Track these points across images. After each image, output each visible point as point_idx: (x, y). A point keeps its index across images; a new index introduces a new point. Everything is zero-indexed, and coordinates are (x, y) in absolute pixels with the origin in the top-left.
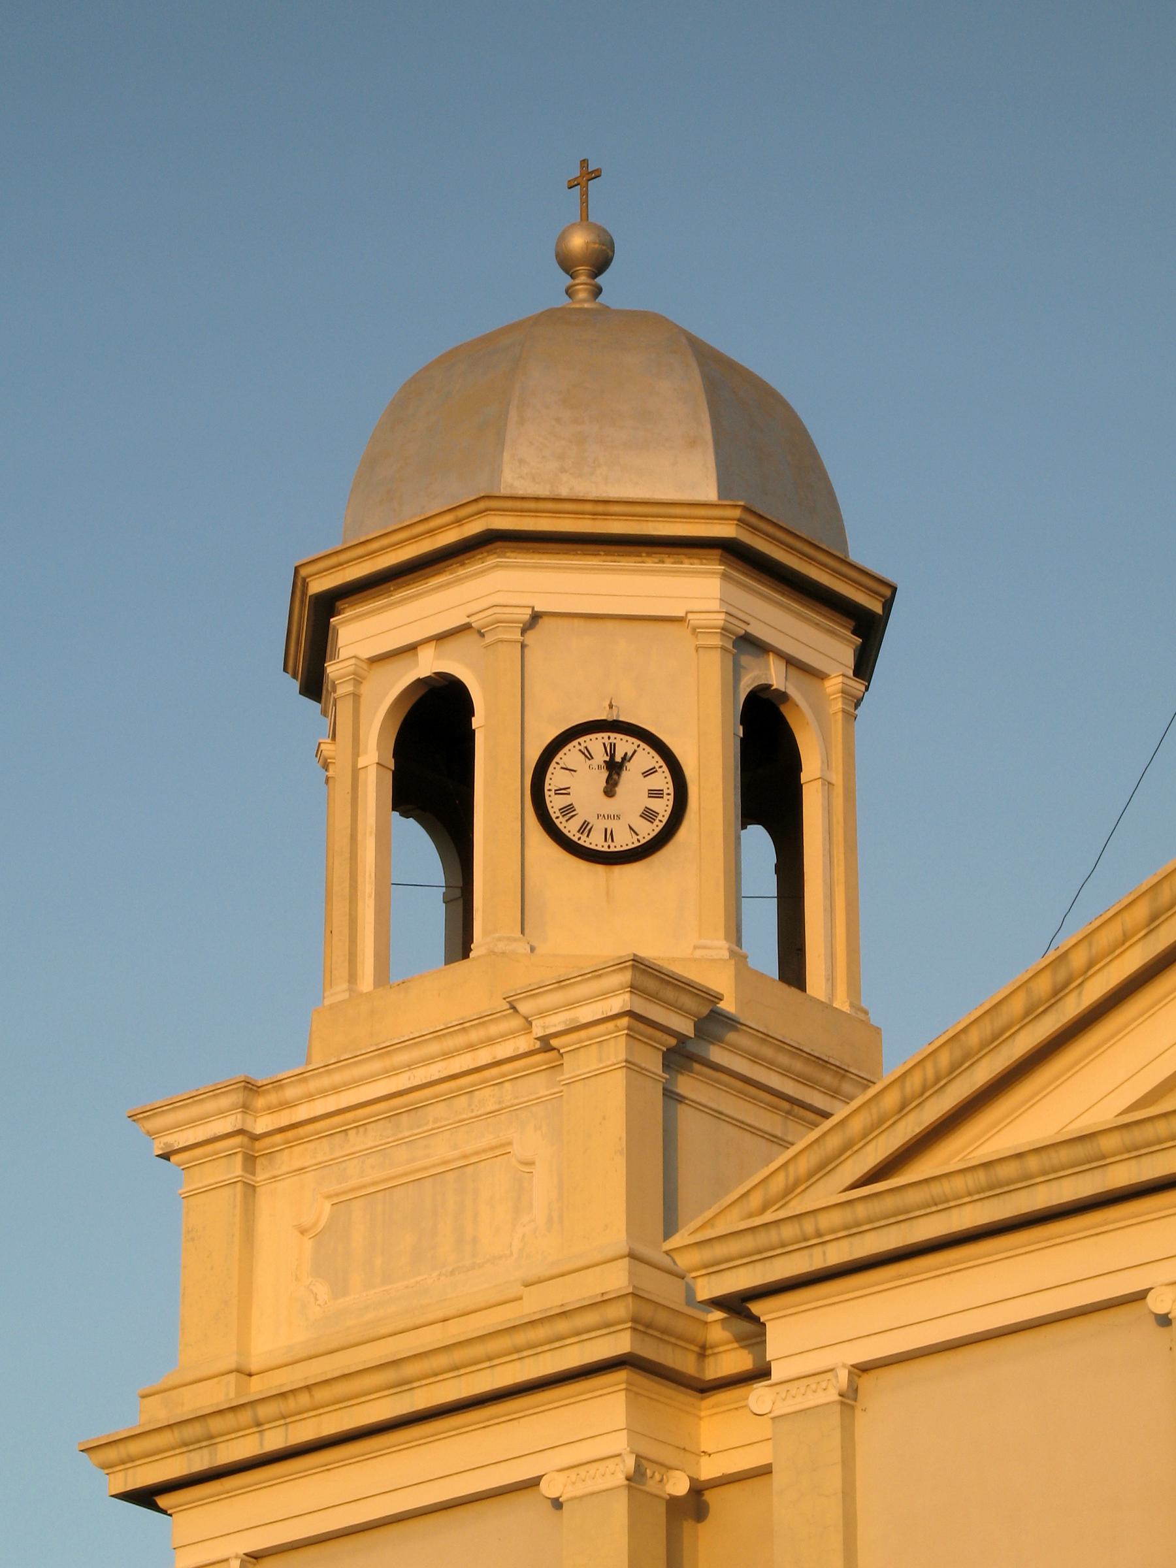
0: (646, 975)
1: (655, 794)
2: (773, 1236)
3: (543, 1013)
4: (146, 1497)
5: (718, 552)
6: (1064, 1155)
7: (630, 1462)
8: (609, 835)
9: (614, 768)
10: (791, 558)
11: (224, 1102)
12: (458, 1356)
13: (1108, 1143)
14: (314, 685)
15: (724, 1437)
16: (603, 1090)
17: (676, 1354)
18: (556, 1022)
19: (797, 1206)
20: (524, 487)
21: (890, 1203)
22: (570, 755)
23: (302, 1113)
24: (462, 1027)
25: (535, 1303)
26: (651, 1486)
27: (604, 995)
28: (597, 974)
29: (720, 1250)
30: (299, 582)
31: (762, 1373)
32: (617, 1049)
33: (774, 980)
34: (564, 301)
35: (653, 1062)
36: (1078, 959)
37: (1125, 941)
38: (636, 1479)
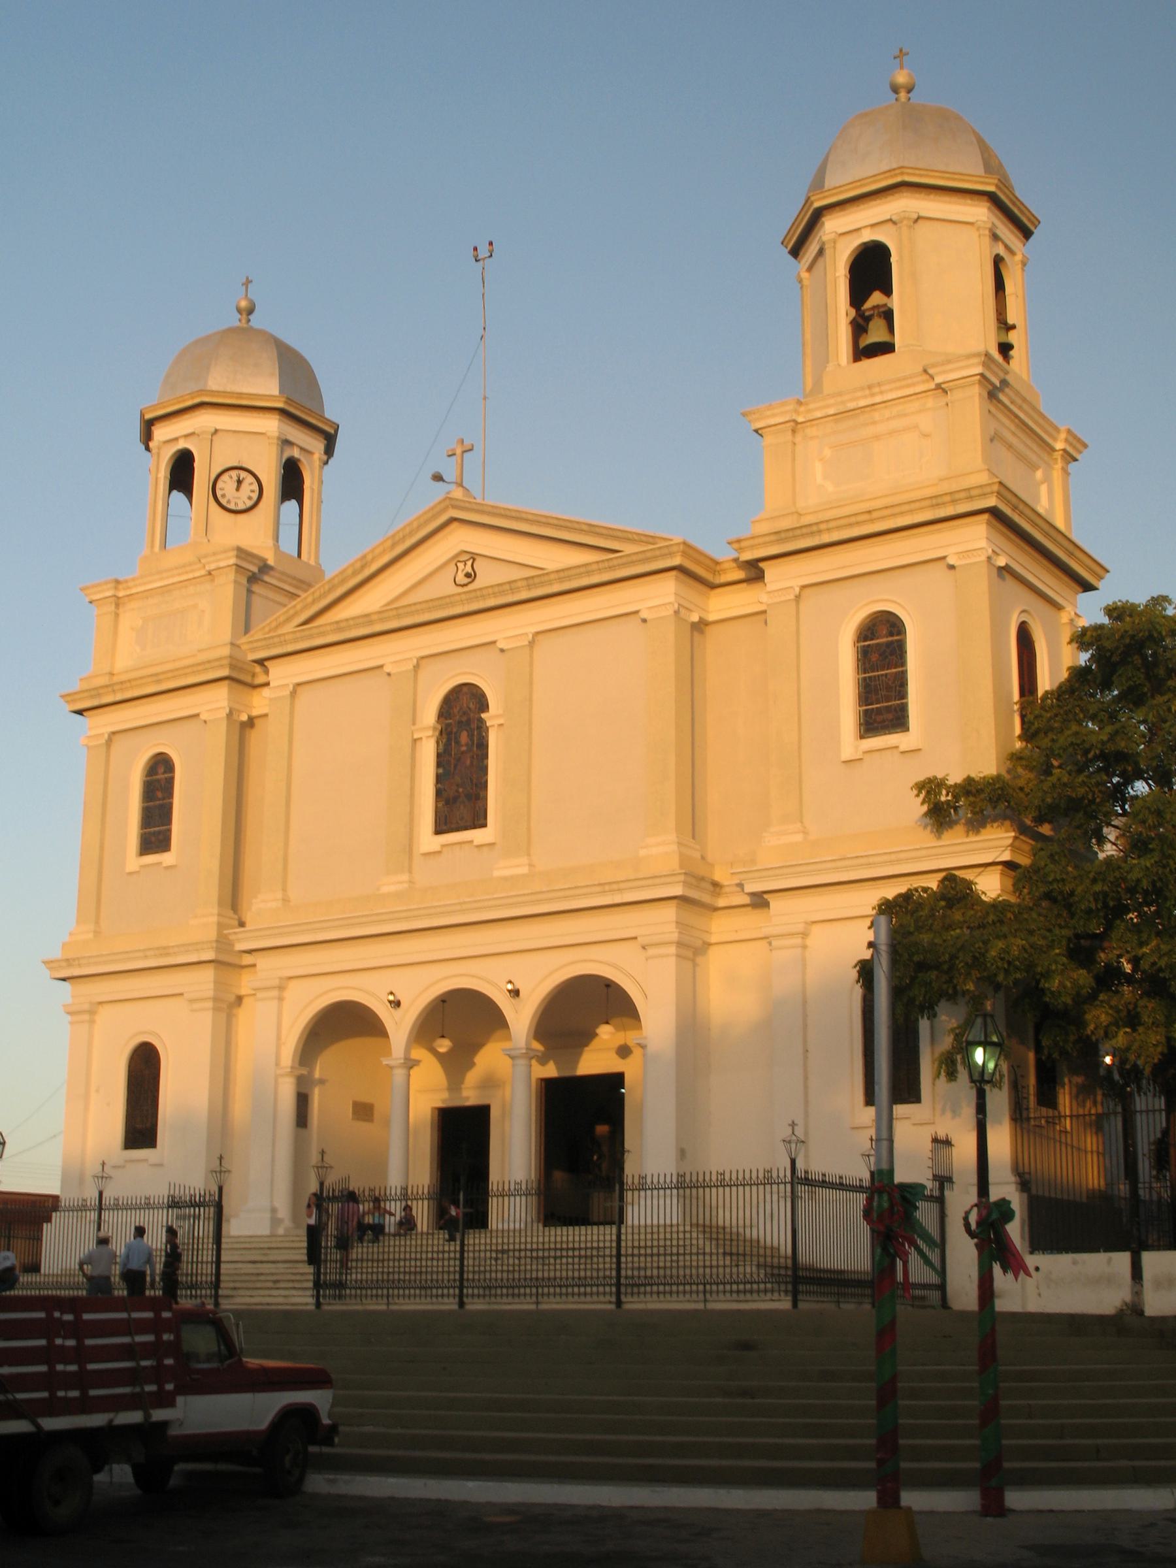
0: (241, 553)
1: (253, 491)
2: (271, 641)
3: (209, 563)
4: (80, 712)
5: (985, 198)
6: (361, 620)
7: (676, 606)
8: (236, 504)
9: (239, 482)
10: (303, 412)
11: (109, 586)
12: (176, 673)
13: (374, 617)
14: (148, 449)
15: (259, 703)
16: (227, 589)
17: (243, 676)
18: (213, 566)
19: (280, 632)
20: (214, 388)
21: (307, 633)
22: (225, 477)
23: (134, 591)
24: (184, 566)
25: (202, 657)
26: (235, 717)
27: (228, 558)
28: (225, 552)
29: (255, 645)
30: (142, 415)
31: (267, 684)
32: (232, 576)
33: (291, 556)
34: (238, 324)
35: (244, 581)
36: (370, 557)
37: (384, 552)
38: (677, 612)
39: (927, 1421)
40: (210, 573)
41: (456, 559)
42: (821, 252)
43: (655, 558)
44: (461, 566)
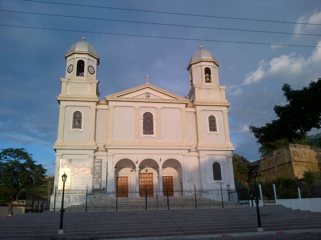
39: (130, 234)
40: (91, 83)
41: (146, 93)
42: (192, 70)
43: (184, 101)
44: (147, 94)
